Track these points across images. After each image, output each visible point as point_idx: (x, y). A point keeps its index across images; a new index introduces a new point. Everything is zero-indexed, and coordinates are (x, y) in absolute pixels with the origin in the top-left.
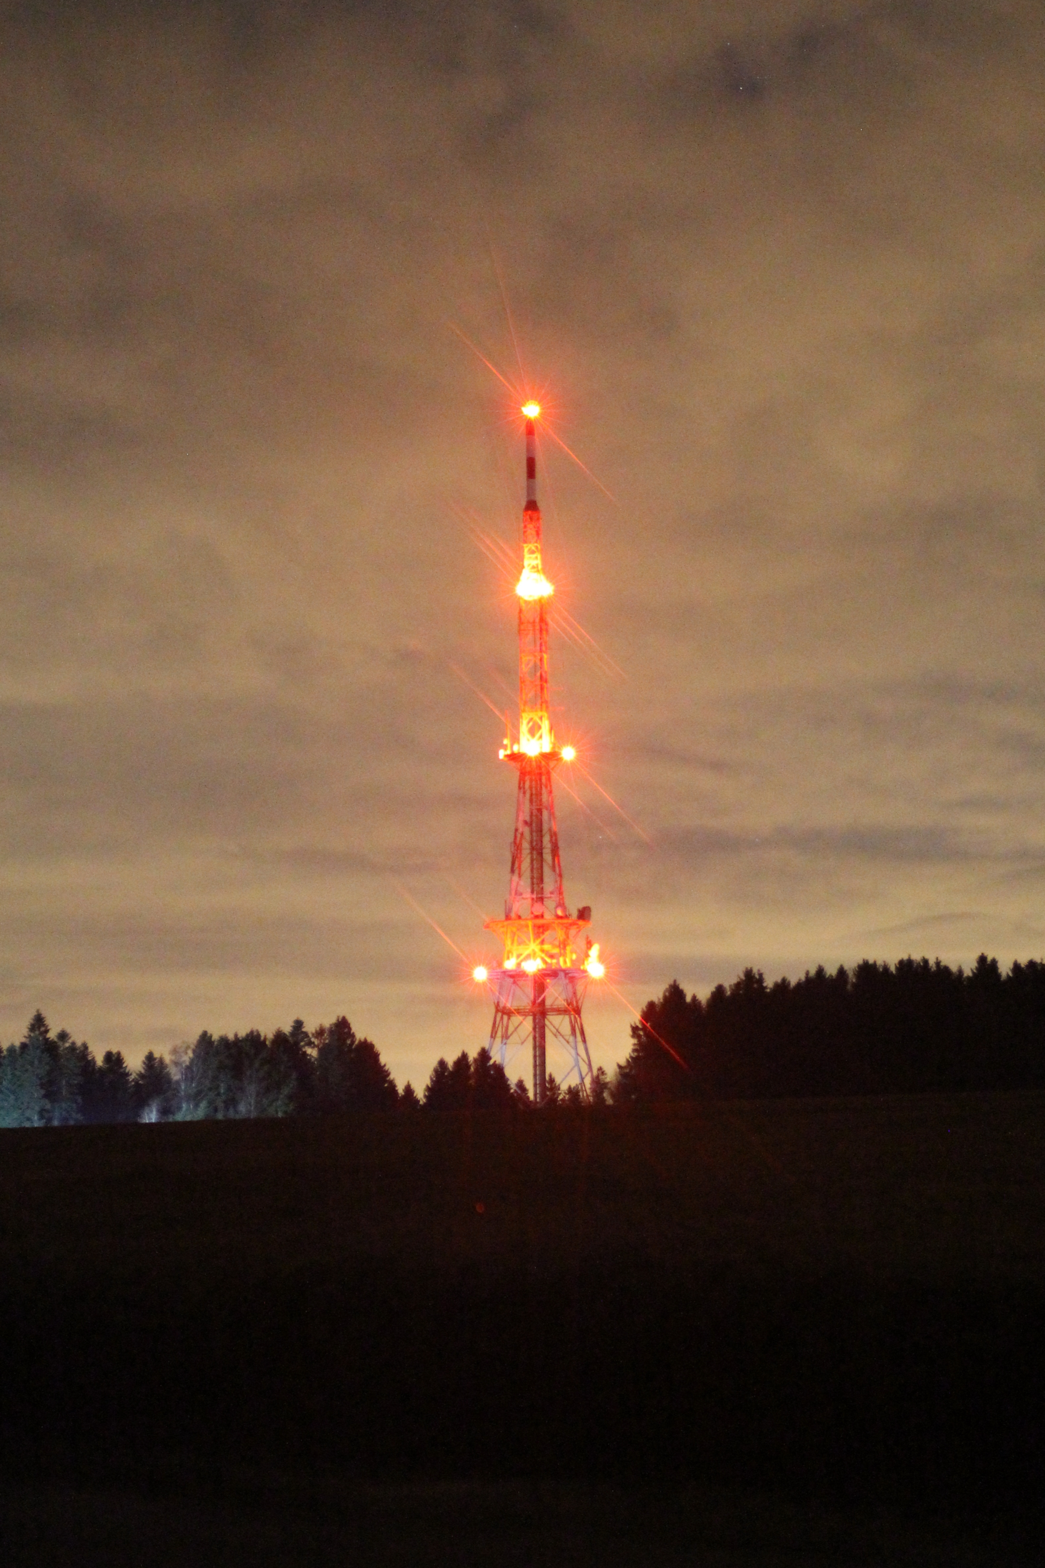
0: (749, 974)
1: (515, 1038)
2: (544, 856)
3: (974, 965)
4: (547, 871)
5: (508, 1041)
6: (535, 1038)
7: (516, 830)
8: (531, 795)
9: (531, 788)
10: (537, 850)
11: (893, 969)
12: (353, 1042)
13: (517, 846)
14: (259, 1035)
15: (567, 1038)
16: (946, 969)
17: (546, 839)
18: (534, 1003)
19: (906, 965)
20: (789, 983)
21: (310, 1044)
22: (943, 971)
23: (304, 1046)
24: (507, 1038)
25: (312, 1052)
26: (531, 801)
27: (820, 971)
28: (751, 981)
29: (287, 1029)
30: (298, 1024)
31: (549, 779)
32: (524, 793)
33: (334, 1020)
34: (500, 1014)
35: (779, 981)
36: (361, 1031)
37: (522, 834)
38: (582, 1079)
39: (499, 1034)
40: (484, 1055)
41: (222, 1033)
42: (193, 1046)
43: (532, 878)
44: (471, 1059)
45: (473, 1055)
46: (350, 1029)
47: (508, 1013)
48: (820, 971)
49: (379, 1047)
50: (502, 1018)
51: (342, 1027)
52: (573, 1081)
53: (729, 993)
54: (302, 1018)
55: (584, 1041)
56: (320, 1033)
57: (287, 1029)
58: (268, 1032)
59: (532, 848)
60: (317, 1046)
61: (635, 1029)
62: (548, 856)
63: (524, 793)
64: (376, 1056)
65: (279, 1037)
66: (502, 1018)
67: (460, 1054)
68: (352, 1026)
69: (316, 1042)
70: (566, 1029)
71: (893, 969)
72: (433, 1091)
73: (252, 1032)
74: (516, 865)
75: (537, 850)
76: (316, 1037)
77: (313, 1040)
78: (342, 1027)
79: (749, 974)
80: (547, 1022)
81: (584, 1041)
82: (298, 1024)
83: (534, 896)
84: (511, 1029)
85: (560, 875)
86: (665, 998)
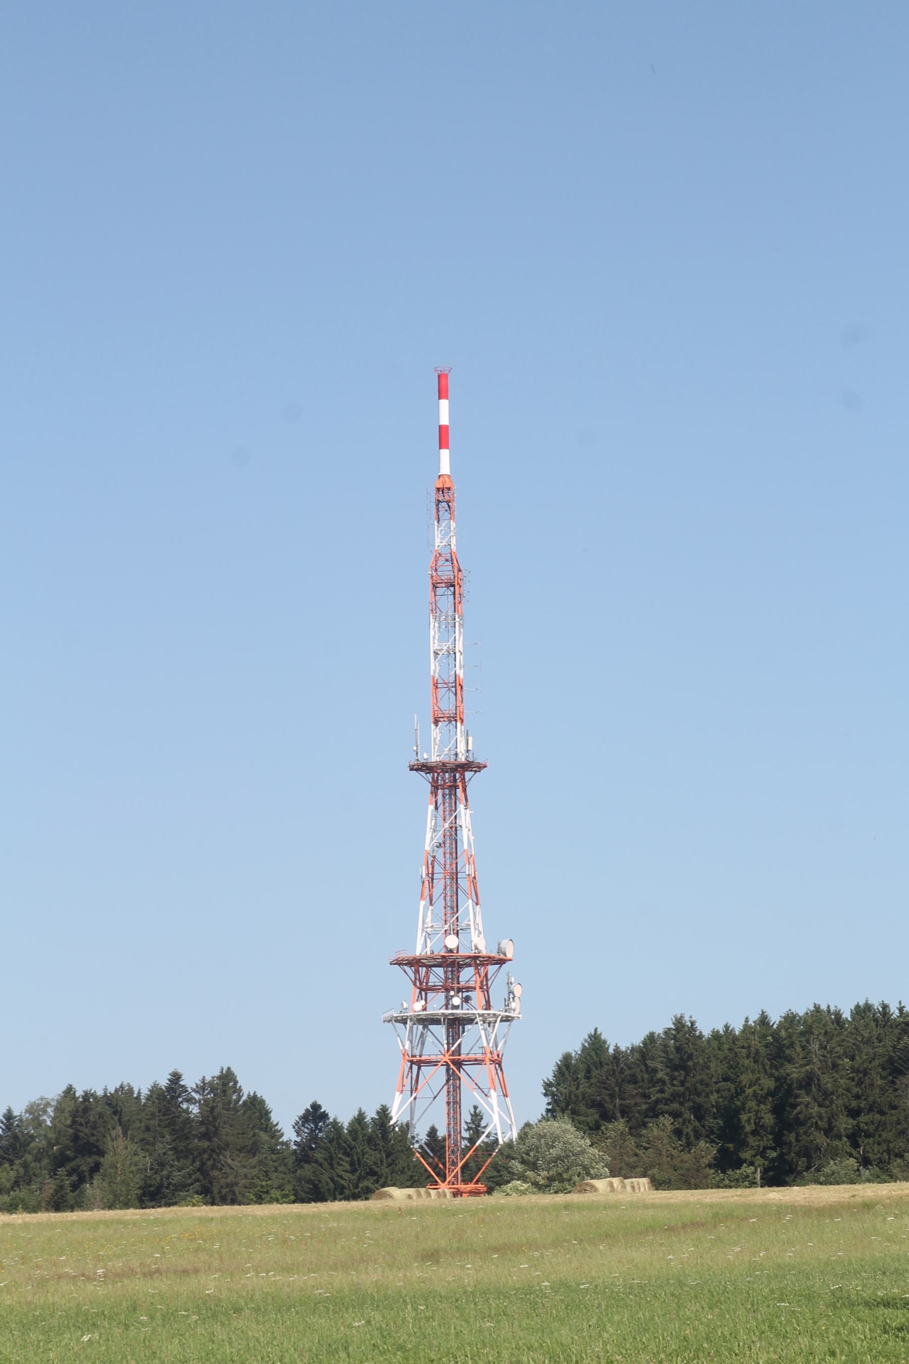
14: (131, 1090)
19: (862, 1011)
21: (190, 1100)
23: (181, 1102)
25: (195, 1110)
27: (763, 1020)
28: (682, 1031)
30: (176, 1078)
33: (217, 1073)
34: (415, 1068)
35: (163, 1082)
36: (248, 1086)
41: (87, 1087)
42: (54, 1103)
44: (368, 1119)
46: (236, 1082)
48: (763, 1020)
51: (227, 1079)
52: (443, 1135)
54: (180, 1071)
56: (202, 1088)
57: (164, 1082)
67: (356, 1113)
68: (97, 1080)
69: (197, 1096)
76: (196, 1092)
77: (193, 1094)
78: (227, 1079)
82: (176, 1078)
86: (584, 1049)
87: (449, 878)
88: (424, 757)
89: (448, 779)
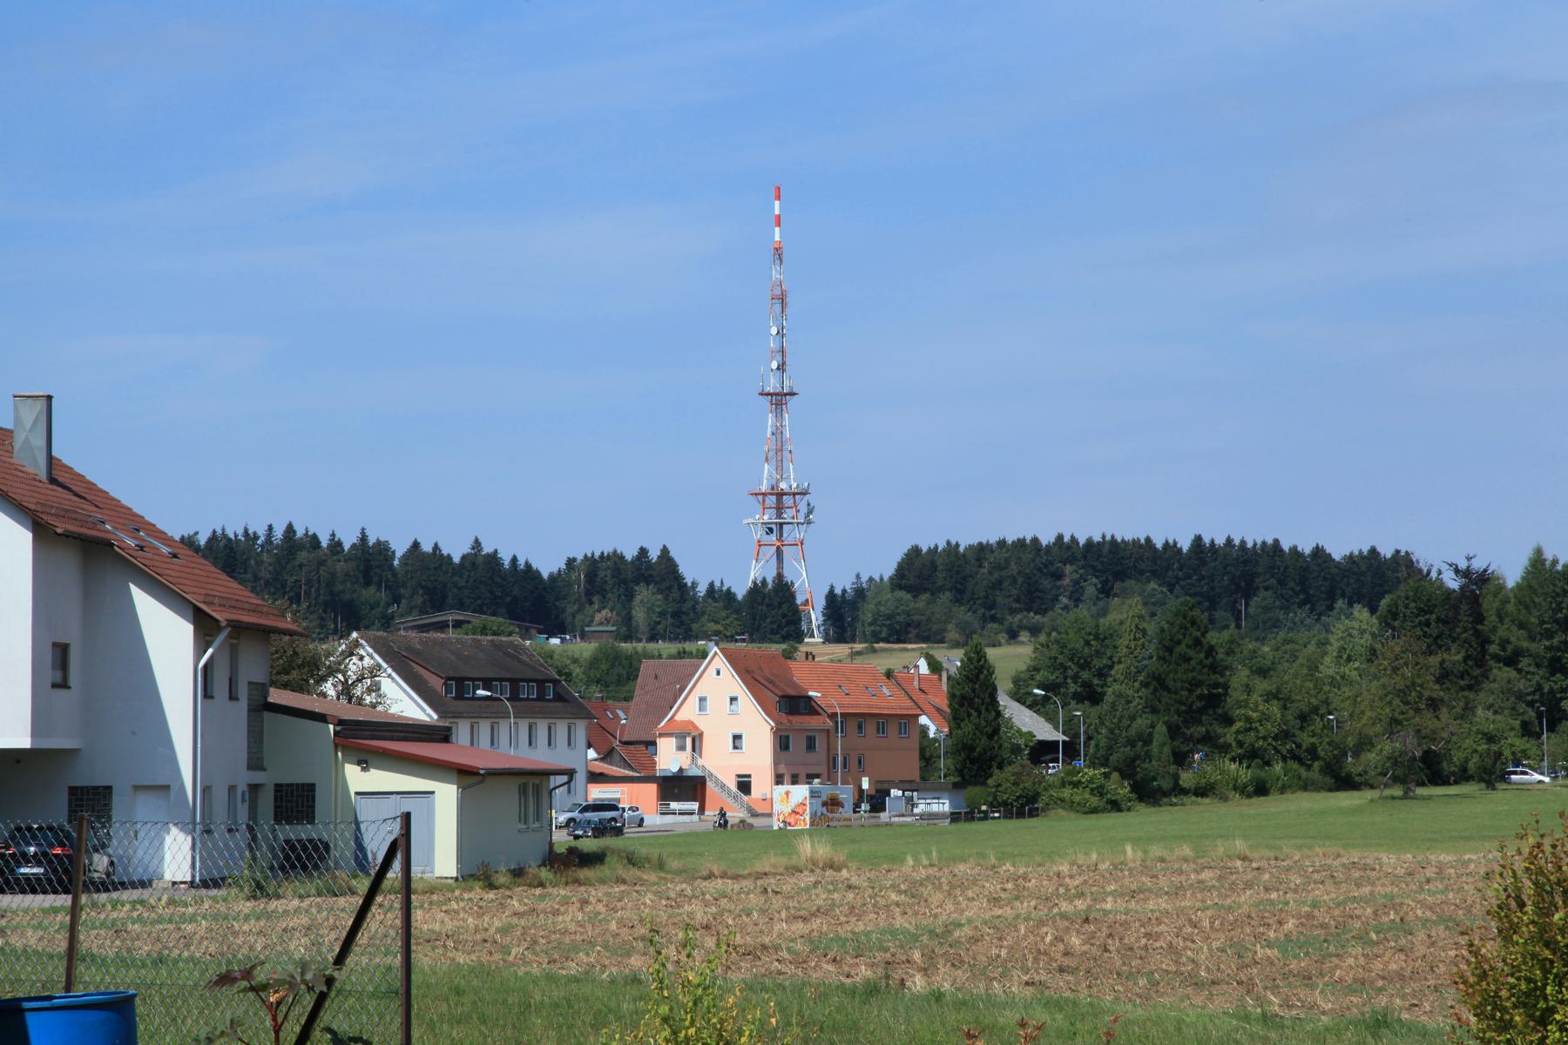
87: (779, 453)
88: (768, 389)
89: (779, 399)
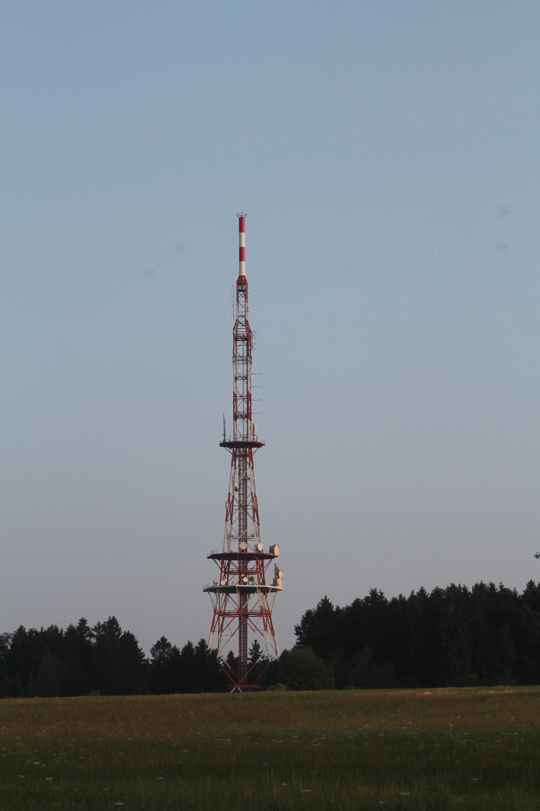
0: (373, 593)
1: (226, 632)
2: (248, 511)
3: (525, 588)
4: (249, 521)
5: (223, 634)
6: (240, 632)
7: (229, 494)
8: (240, 470)
9: (239, 465)
10: (243, 507)
11: (470, 590)
12: (120, 634)
13: (230, 503)
14: (57, 629)
15: (262, 632)
16: (507, 590)
17: (249, 499)
18: (240, 608)
19: (480, 588)
20: (396, 599)
21: (91, 635)
22: (505, 592)
24: (222, 631)
26: (240, 474)
29: (76, 624)
30: (83, 622)
31: (251, 459)
32: (235, 468)
34: (217, 616)
37: (233, 497)
38: (240, 654)
39: (217, 629)
40: (203, 643)
41: (31, 627)
43: (240, 525)
45: (195, 644)
46: (118, 625)
47: (224, 615)
49: (137, 637)
50: (219, 618)
51: (113, 622)
53: (537, 586)
55: (273, 634)
56: (98, 627)
57: (76, 624)
58: (63, 627)
59: (240, 506)
60: (96, 636)
61: (297, 629)
62: (250, 511)
63: (235, 468)
64: (135, 643)
65: (71, 629)
66: (219, 618)
67: (187, 643)
70: (261, 627)
71: (470, 590)
72: (67, 634)
73: (52, 627)
74: (254, 499)
75: (243, 507)
77: (93, 632)
79: (373, 593)
80: (248, 621)
81: (273, 634)
82: (83, 622)
83: (241, 537)
84: (225, 625)
85: (258, 524)
